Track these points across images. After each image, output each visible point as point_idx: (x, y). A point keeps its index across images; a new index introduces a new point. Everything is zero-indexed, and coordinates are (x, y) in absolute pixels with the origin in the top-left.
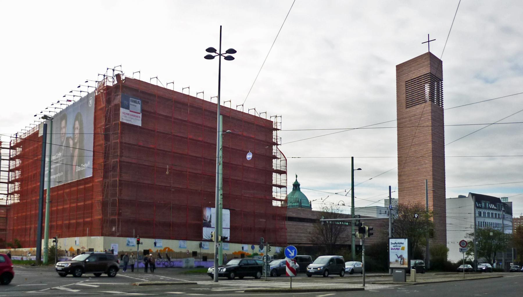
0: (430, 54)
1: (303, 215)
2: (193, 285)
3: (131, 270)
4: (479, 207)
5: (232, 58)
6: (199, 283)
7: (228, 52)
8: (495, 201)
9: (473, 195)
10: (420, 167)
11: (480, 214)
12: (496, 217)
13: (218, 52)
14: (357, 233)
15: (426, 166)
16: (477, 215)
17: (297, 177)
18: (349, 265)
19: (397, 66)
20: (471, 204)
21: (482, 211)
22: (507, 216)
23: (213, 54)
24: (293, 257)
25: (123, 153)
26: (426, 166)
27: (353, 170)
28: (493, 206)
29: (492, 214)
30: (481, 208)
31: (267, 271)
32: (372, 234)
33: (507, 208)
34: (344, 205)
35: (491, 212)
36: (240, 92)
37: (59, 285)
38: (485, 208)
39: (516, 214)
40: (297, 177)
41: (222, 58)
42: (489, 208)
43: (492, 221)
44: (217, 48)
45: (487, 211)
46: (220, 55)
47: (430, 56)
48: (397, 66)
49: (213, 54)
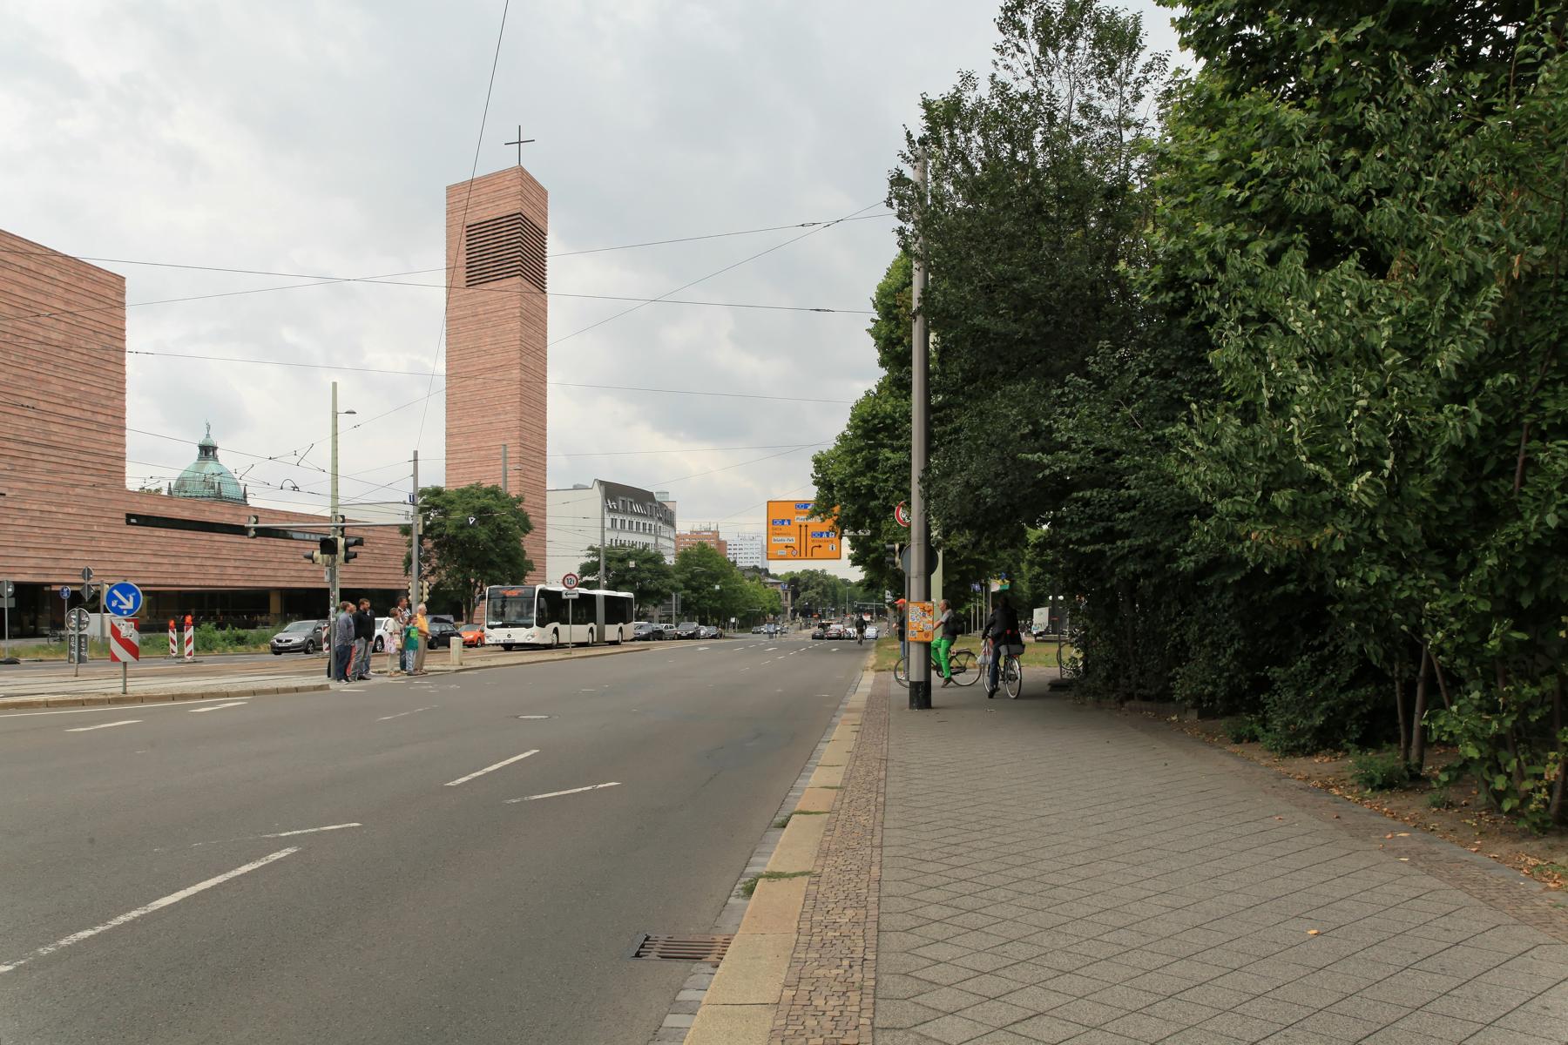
0: (521, 171)
3: (840, 590)
4: (611, 510)
9: (601, 483)
10: (492, 419)
11: (614, 521)
12: (646, 530)
15: (508, 417)
16: (608, 524)
17: (209, 428)
19: (448, 188)
20: (597, 494)
21: (619, 518)
24: (129, 611)
26: (508, 417)
27: (335, 415)
28: (637, 508)
31: (80, 650)
35: (635, 520)
38: (625, 512)
39: (684, 526)
40: (209, 428)
42: (633, 513)
45: (627, 519)
48: (452, 191)
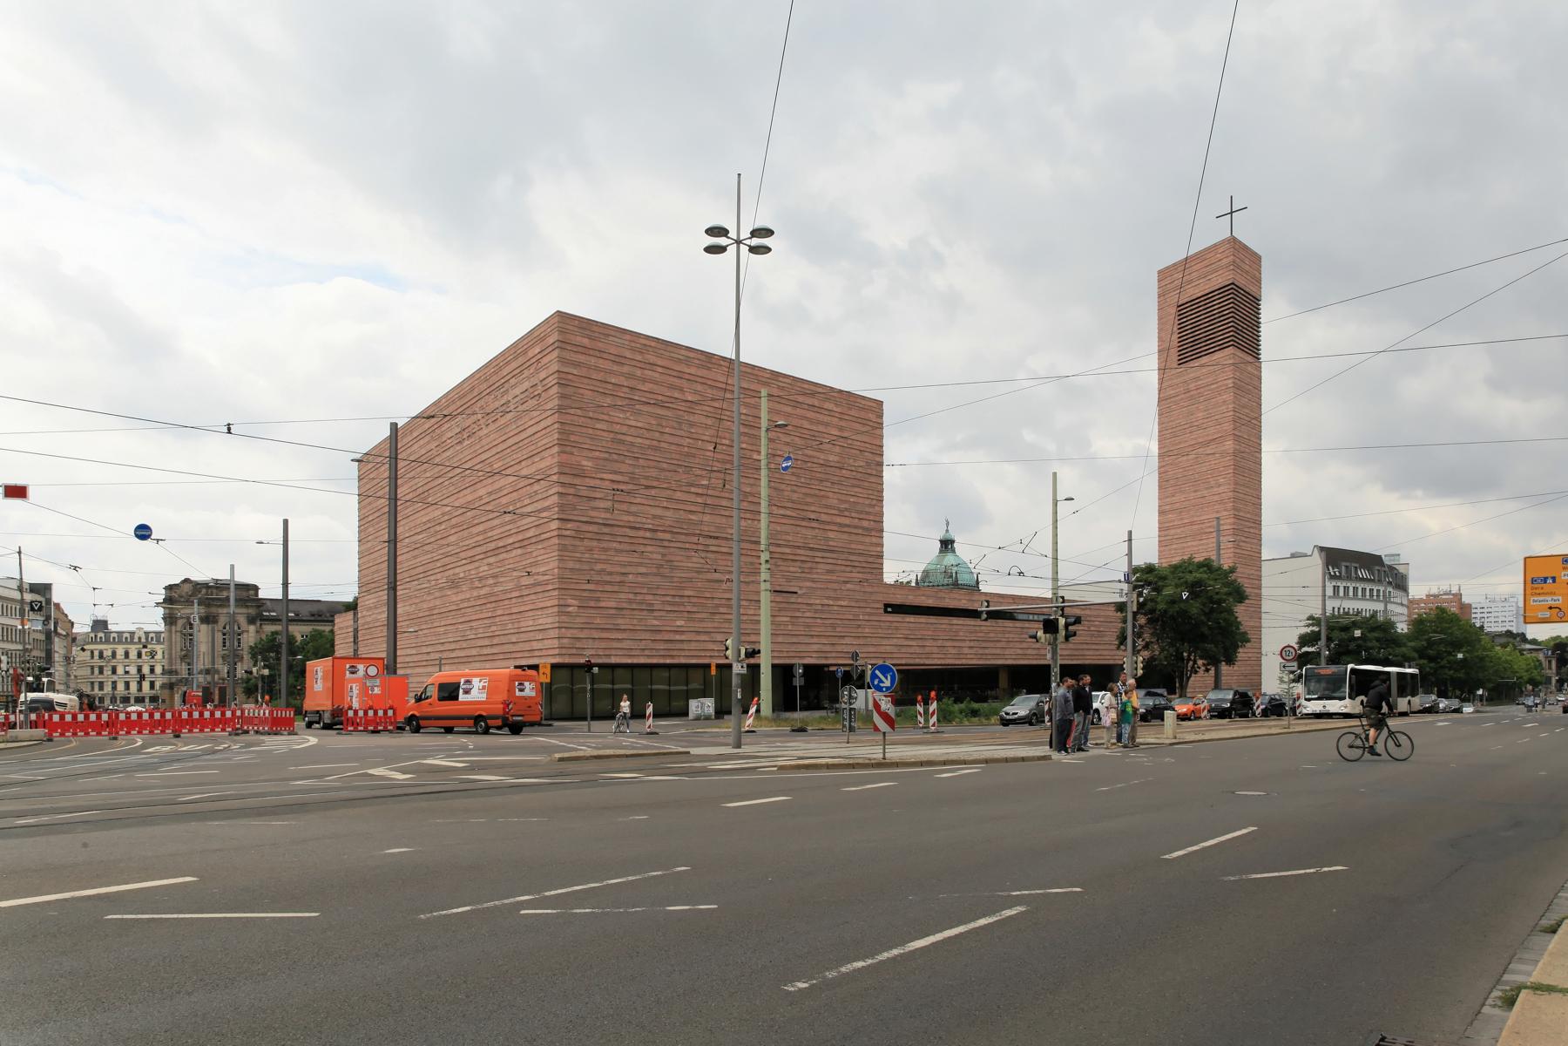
1: (964, 603)
2: (684, 757)
4: (1333, 577)
5: (767, 250)
6: (694, 751)
7: (755, 233)
8: (1370, 562)
9: (1322, 549)
11: (1336, 588)
13: (732, 234)
14: (1040, 633)
15: (1221, 489)
16: (1329, 592)
18: (694, 706)
20: (1317, 561)
21: (1342, 585)
22: (1394, 592)
23: (722, 241)
25: (1319, 681)
26: (1221, 489)
28: (1363, 573)
29: (1364, 590)
30: (1339, 578)
32: (1075, 634)
33: (1400, 583)
34: (1021, 573)
35: (1360, 586)
36: (791, 328)
37: (425, 758)
38: (1349, 578)
41: (744, 249)
43: (1361, 604)
44: (731, 227)
46: (738, 242)
47: (1234, 243)
49: (722, 241)
